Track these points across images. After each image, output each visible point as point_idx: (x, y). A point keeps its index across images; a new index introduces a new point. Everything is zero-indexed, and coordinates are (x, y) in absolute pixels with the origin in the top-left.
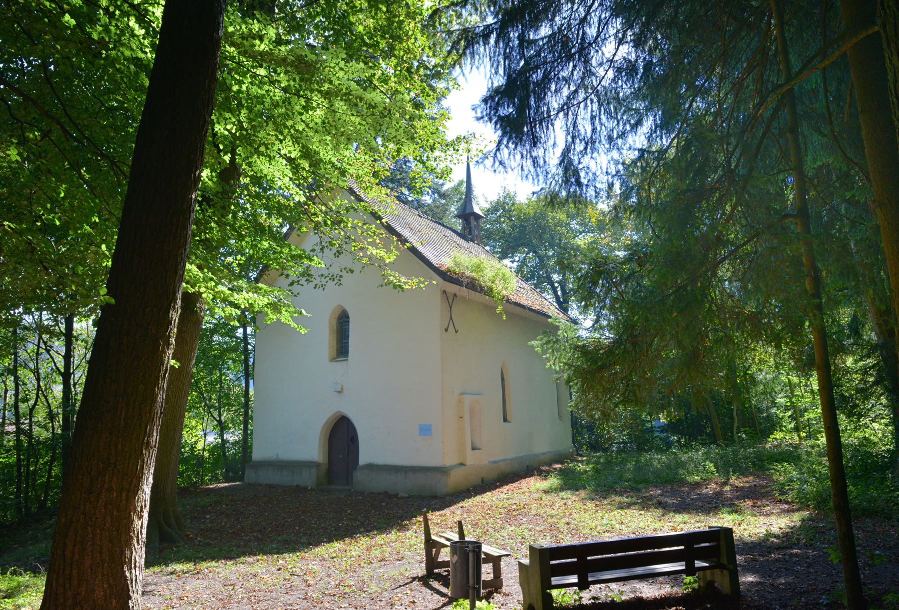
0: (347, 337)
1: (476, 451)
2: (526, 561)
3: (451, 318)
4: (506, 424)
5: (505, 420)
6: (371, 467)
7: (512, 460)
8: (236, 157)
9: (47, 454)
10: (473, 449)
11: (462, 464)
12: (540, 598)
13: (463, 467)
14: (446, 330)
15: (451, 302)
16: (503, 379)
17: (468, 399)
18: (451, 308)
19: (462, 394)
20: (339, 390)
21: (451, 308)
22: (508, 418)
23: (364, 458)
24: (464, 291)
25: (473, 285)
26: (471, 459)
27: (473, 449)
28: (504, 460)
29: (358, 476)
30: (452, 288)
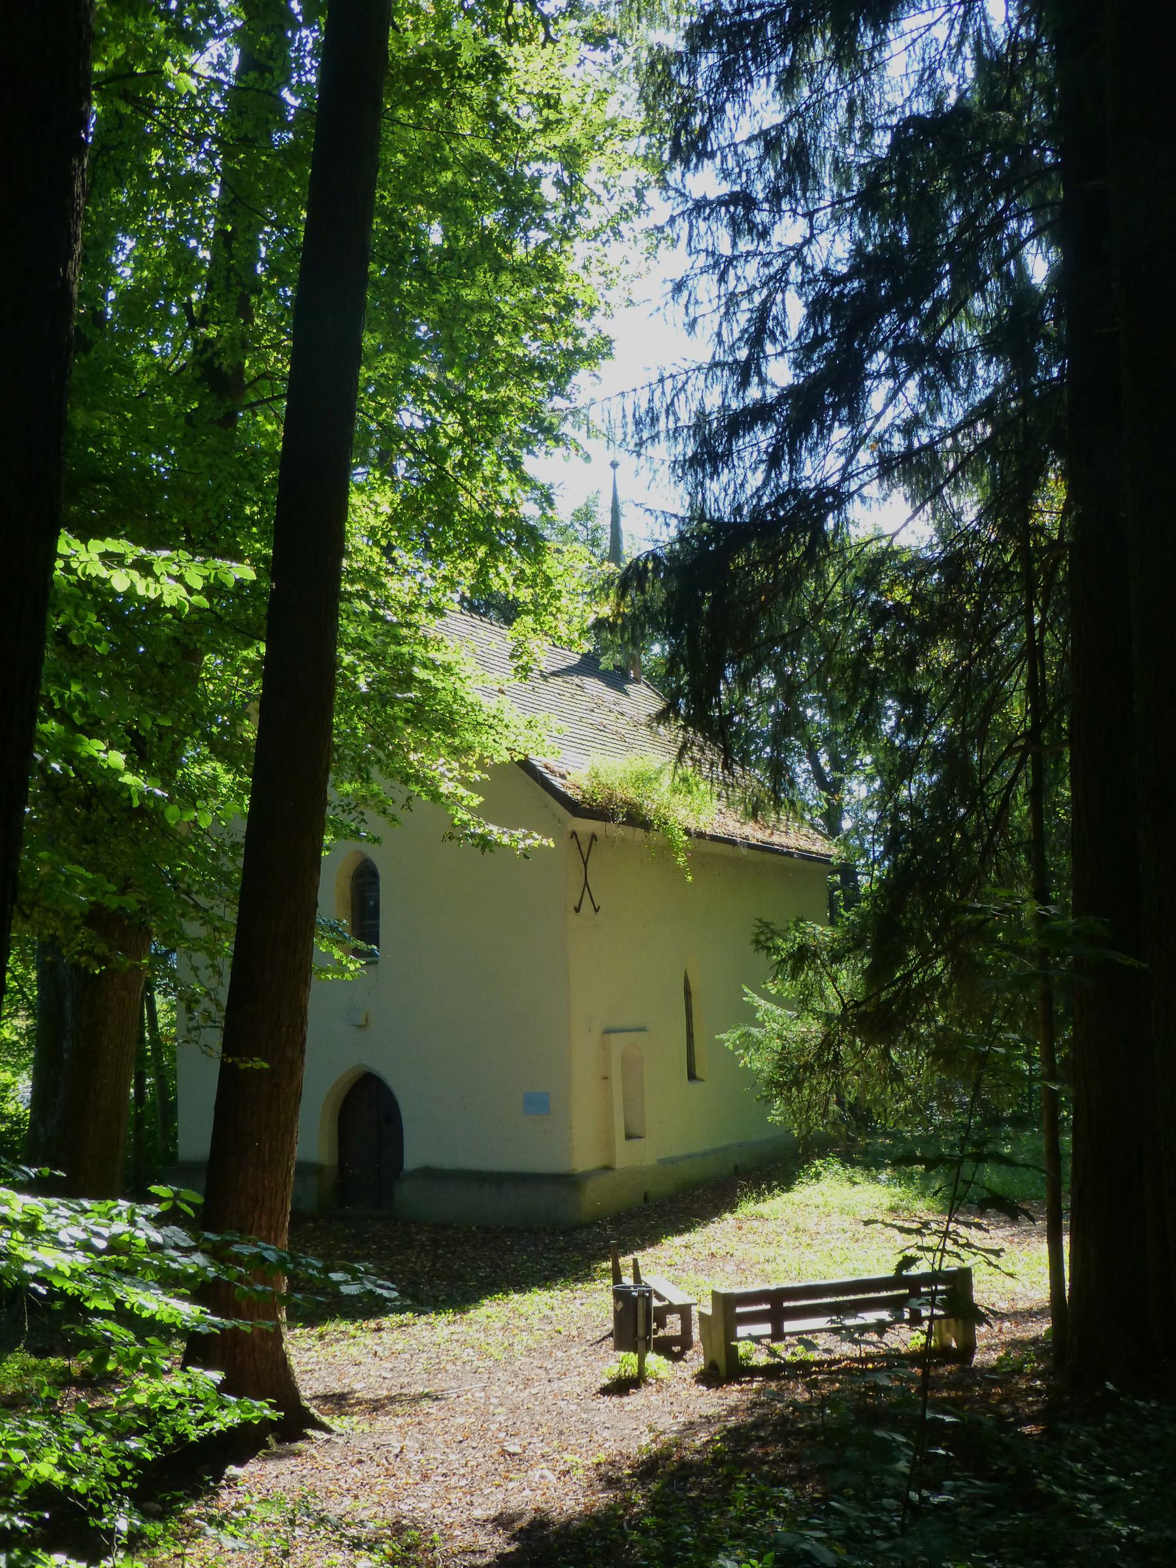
0: (375, 913)
1: (635, 1142)
2: (709, 1311)
3: (586, 884)
4: (695, 1085)
5: (692, 1076)
6: (429, 1174)
7: (705, 1154)
8: (916, 444)
9: (783, 52)
10: (629, 1137)
11: (608, 1168)
12: (723, 1352)
13: (610, 1173)
14: (577, 910)
15: (585, 850)
16: (688, 993)
17: (618, 1043)
18: (585, 863)
19: (608, 1032)
20: (363, 1022)
21: (585, 863)
22: (698, 1073)
23: (414, 1157)
24: (616, 830)
25: (636, 818)
26: (626, 1156)
27: (629, 1137)
28: (689, 1157)
29: (404, 1192)
30: (585, 826)
